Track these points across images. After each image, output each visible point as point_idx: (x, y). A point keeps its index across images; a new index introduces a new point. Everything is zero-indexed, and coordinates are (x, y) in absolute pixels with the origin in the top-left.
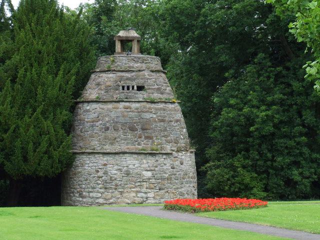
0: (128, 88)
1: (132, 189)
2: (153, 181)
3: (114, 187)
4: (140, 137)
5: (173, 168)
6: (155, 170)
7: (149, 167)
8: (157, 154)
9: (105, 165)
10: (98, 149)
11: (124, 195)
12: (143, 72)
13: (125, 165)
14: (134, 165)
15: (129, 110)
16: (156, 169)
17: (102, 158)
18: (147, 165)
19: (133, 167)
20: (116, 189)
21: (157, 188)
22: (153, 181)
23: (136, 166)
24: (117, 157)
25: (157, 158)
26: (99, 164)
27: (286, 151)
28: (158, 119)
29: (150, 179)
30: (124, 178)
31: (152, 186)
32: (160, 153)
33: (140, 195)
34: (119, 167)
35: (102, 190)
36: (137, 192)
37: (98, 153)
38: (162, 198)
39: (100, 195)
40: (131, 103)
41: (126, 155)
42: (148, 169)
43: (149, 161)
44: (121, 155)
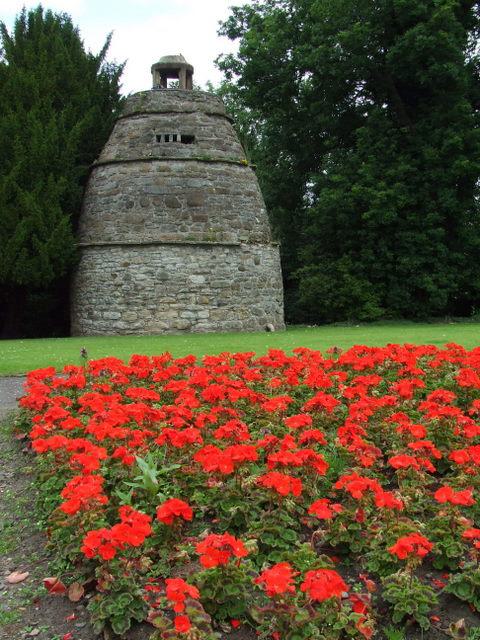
2: (207, 290)
7: (200, 267)
11: (158, 315)
14: (174, 264)
15: (166, 173)
17: (120, 253)
18: (197, 265)
22: (207, 290)
25: (214, 253)
29: (201, 288)
32: (219, 245)
33: (184, 314)
44: (153, 248)
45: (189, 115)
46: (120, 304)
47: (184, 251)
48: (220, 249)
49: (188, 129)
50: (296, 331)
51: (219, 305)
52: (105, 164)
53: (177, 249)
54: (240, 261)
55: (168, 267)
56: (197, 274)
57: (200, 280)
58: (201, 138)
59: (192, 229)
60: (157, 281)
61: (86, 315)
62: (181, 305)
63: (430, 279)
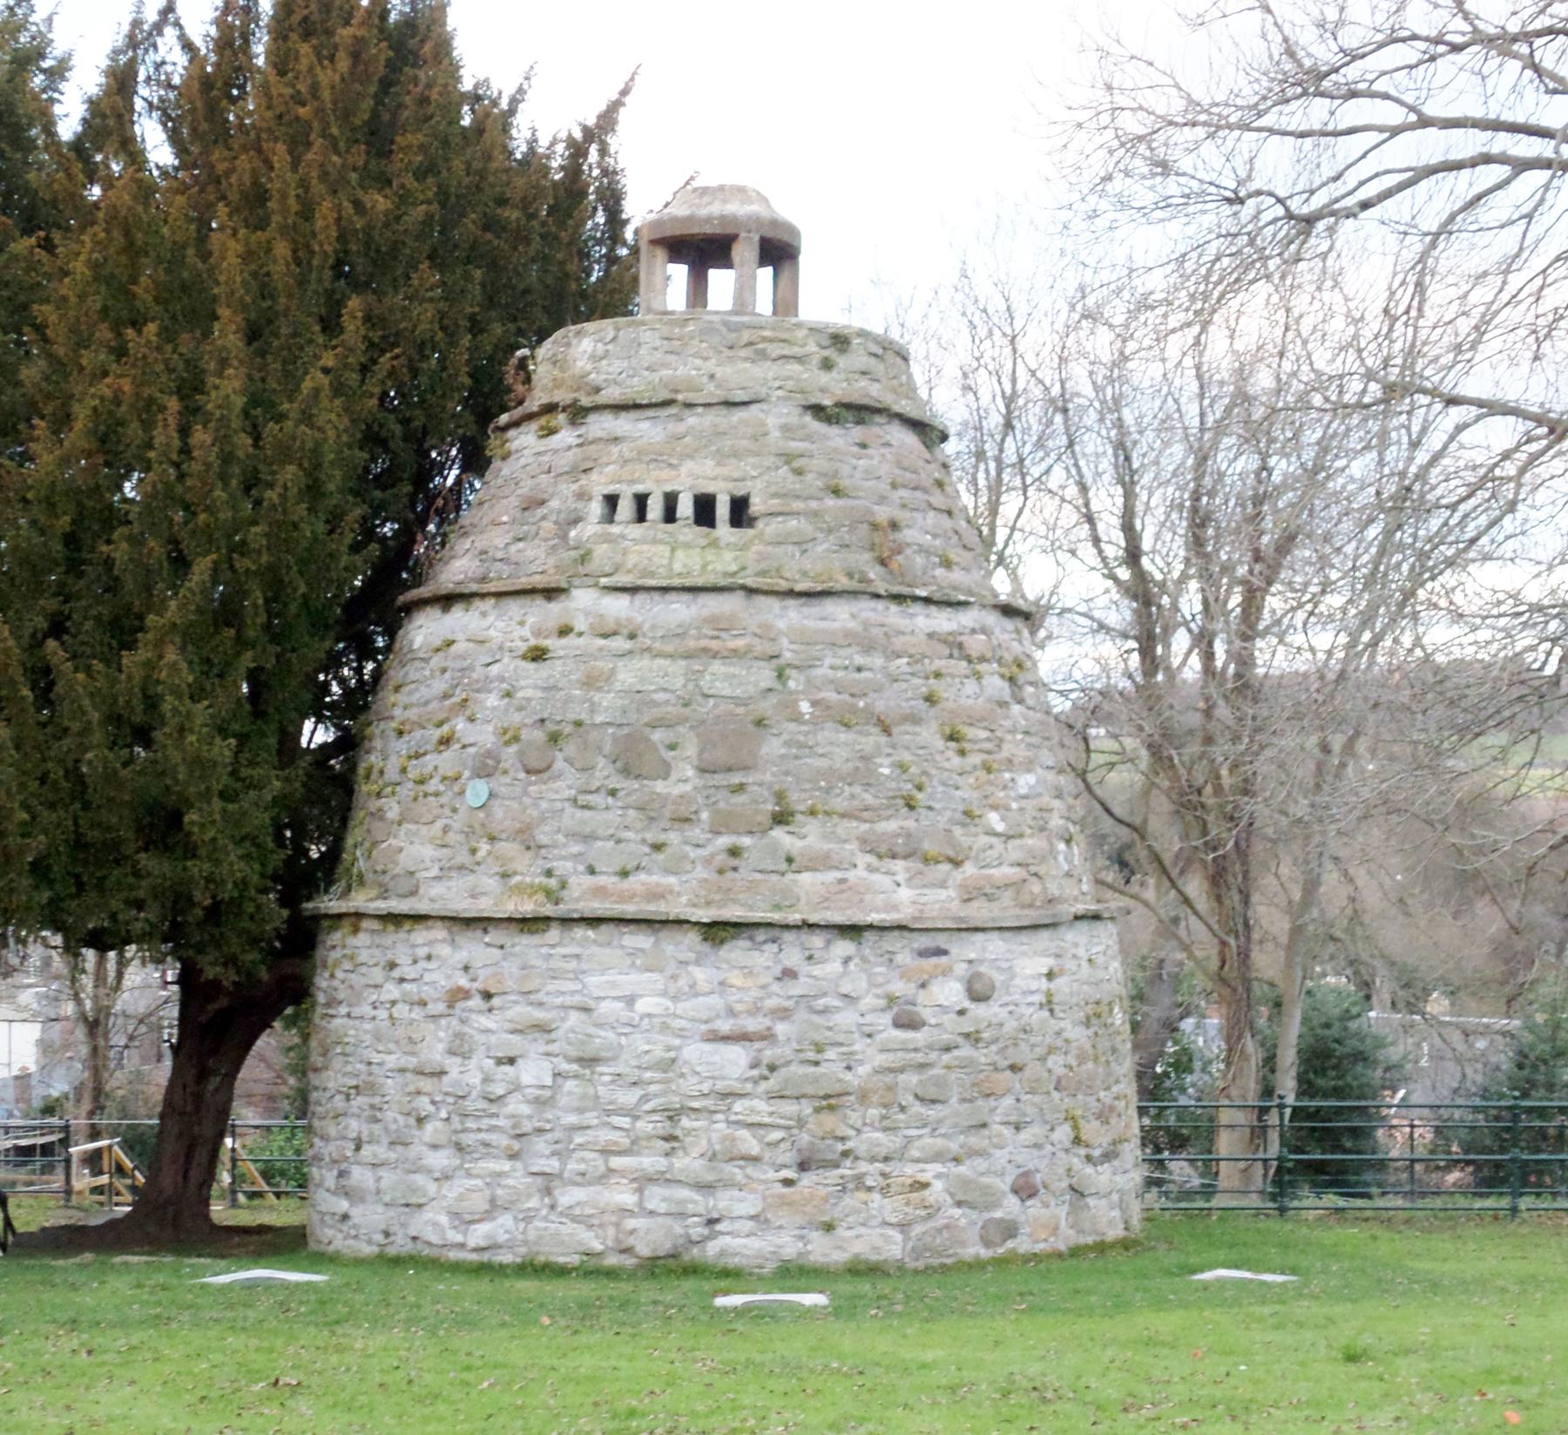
1: (616, 1162)
2: (759, 1108)
3: (505, 1141)
5: (909, 1022)
7: (731, 1013)
10: (580, 896)
11: (568, 1197)
14: (630, 1000)
15: (620, 644)
16: (781, 1028)
17: (444, 950)
18: (715, 1001)
19: (625, 1015)
20: (513, 1156)
22: (759, 1108)
23: (642, 1006)
25: (792, 956)
27: (152, 454)
28: (814, 704)
30: (570, 1085)
33: (657, 1198)
34: (540, 1015)
36: (643, 1181)
42: (725, 1026)
43: (736, 978)
45: (738, 415)
47: (669, 949)
51: (803, 1166)
52: (447, 601)
55: (605, 1007)
60: (565, 1066)
61: (330, 1179)
63: (1102, 731)
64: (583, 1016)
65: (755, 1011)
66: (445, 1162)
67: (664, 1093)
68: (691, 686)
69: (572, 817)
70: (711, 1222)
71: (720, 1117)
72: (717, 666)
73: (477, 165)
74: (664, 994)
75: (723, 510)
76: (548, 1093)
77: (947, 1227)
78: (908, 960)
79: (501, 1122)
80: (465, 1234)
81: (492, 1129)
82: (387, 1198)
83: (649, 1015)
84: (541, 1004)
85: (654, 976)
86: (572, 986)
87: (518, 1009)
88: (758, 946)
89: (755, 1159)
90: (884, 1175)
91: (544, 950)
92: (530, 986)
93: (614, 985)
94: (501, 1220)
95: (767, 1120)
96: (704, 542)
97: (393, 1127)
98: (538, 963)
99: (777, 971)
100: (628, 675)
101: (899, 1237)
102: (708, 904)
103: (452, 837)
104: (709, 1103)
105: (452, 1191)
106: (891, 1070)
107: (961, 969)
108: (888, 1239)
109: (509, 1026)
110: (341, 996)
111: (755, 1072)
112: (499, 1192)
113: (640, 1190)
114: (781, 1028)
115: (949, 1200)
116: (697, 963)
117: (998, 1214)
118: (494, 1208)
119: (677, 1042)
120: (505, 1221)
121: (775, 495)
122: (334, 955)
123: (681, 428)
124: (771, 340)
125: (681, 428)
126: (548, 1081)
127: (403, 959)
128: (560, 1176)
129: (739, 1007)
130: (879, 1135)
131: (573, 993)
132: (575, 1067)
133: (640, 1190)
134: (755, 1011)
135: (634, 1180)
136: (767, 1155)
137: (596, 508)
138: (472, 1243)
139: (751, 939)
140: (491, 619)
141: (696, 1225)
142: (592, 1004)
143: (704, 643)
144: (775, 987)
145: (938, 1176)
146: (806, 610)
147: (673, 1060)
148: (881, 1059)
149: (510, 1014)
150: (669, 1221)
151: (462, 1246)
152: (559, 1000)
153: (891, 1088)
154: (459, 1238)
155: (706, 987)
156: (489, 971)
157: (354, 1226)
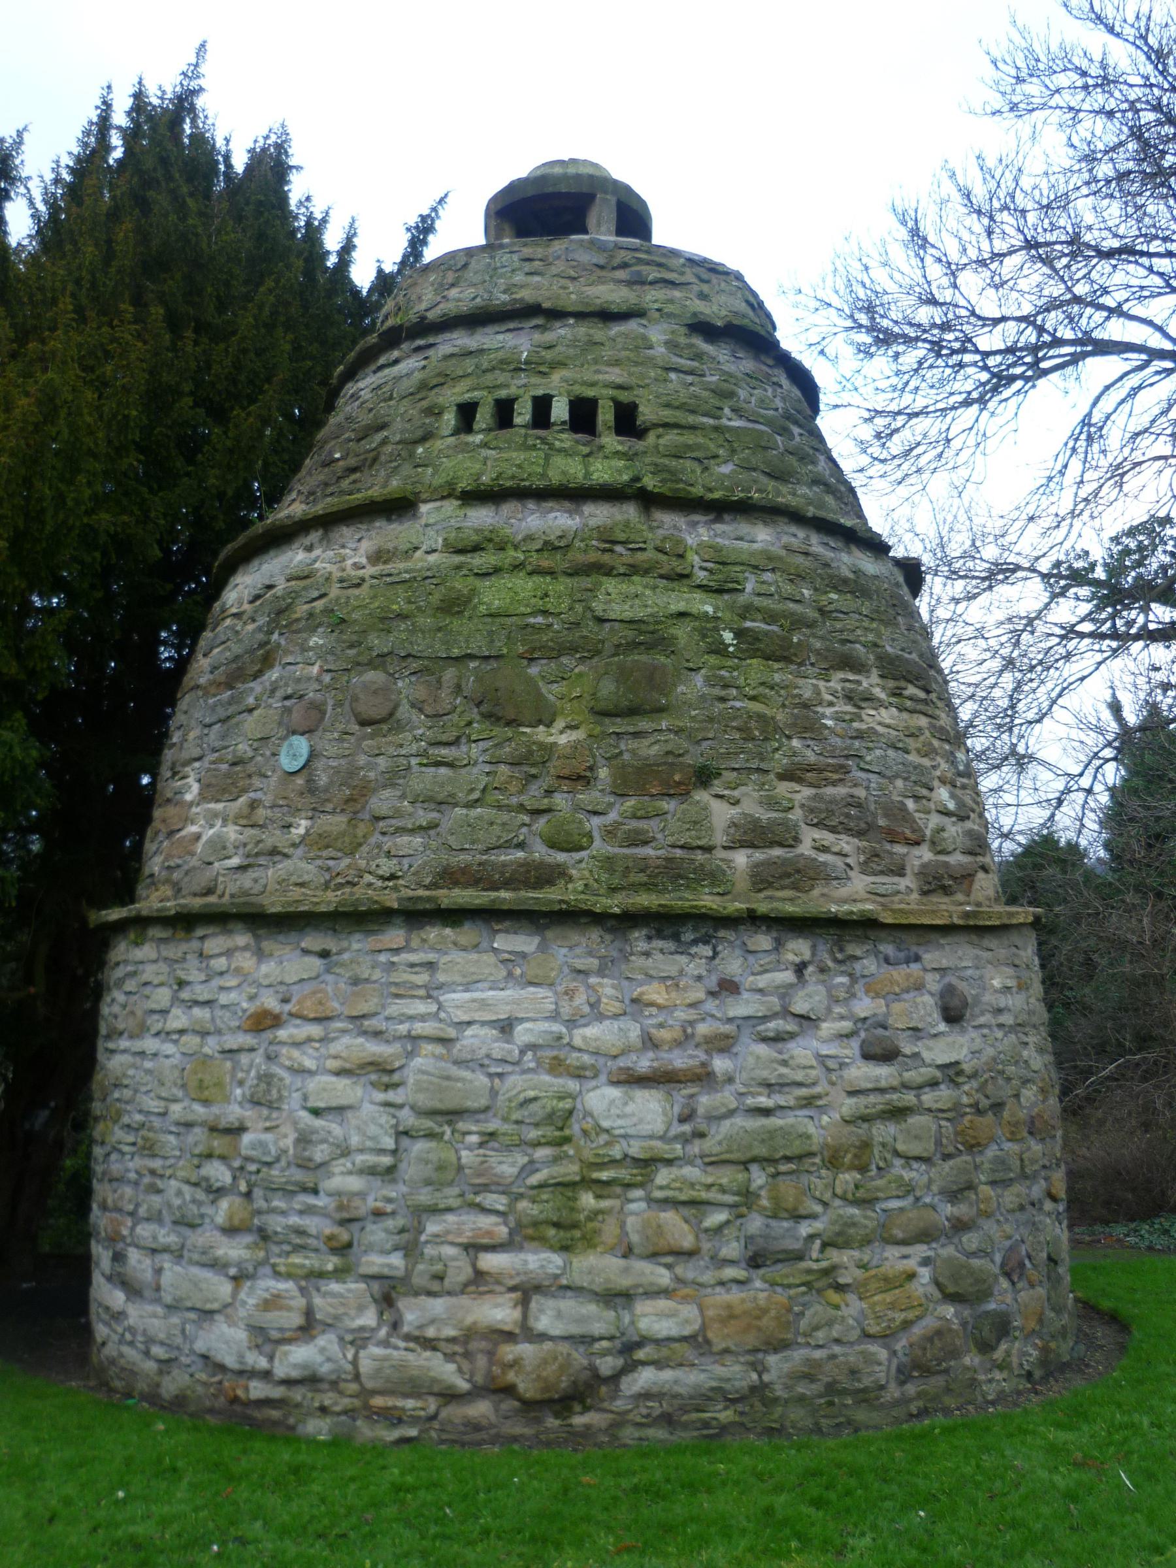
0: (504, 412)
1: (491, 1261)
4: (582, 779)
6: (704, 1077)
8: (731, 922)
9: (263, 1022)
12: (632, 325)
13: (419, 1028)
14: (506, 1027)
16: (720, 1064)
17: (246, 961)
19: (499, 1048)
21: (732, 1249)
23: (523, 1033)
24: (356, 947)
26: (226, 1019)
28: (739, 634)
29: (648, 1163)
30: (419, 1147)
31: (677, 1228)
32: (754, 920)
34: (375, 1049)
35: (234, 1250)
36: (527, 1291)
37: (220, 919)
38: (780, 1346)
39: (225, 1289)
40: (508, 508)
41: (433, 933)
42: (644, 1063)
43: (655, 993)
44: (395, 936)
45: (616, 329)
46: (230, 1231)
48: (763, 941)
49: (603, 379)
50: (281, 938)
53: (523, 942)
54: (864, 1006)
56: (634, 1080)
57: (648, 1114)
58: (667, 415)
59: (610, 833)
62: (538, 1261)
64: (439, 1049)
65: (685, 1039)
66: (244, 1254)
67: (556, 1160)
68: (579, 608)
69: (425, 779)
70: (628, 1348)
71: (638, 1193)
72: (610, 585)
73: (319, 1153)
74: (555, 1016)
75: (605, 415)
76: (387, 1160)
77: (939, 1333)
78: (873, 968)
79: (320, 1202)
80: (271, 1358)
81: (307, 1211)
82: (168, 1299)
83: (533, 1047)
84: (377, 1034)
85: (541, 992)
86: (421, 1007)
87: (346, 1040)
88: (683, 949)
89: (691, 1254)
90: (863, 1266)
91: (383, 958)
92: (363, 1008)
93: (483, 1004)
94: (321, 1341)
95: (704, 1195)
96: (586, 450)
97: (177, 1202)
98: (377, 975)
99: (712, 982)
100: (492, 594)
101: (883, 1354)
102: (613, 890)
103: (261, 813)
104: (623, 1174)
105: (251, 1297)
106: (865, 1119)
107: (933, 983)
108: (870, 1359)
109: (332, 1064)
110: (121, 1026)
111: (687, 1128)
112: (318, 1301)
113: (525, 1303)
114: (720, 1064)
115: (937, 1295)
116: (601, 972)
117: (992, 1306)
118: (309, 1327)
119: (572, 1085)
120: (327, 1341)
121: (668, 405)
122: (119, 972)
123: (549, 337)
124: (648, 263)
125: (549, 337)
126: (389, 1142)
127: (194, 975)
128: (405, 1279)
129: (665, 1034)
130: (854, 1211)
131: (423, 1018)
132: (428, 1124)
133: (525, 1303)
134: (685, 1039)
135: (512, 1289)
136: (706, 1246)
137: (450, 418)
138: (280, 1371)
139: (676, 937)
140: (317, 552)
141: (604, 1353)
142: (452, 1033)
143: (593, 556)
144: (711, 1005)
145: (926, 1262)
146: (719, 527)
147: (571, 1112)
148: (849, 1106)
149: (337, 1047)
150: (564, 1348)
151: (266, 1375)
152: (403, 1028)
153: (866, 1145)
154: (263, 1363)
155: (615, 1007)
156: (308, 988)
157: (130, 1329)
